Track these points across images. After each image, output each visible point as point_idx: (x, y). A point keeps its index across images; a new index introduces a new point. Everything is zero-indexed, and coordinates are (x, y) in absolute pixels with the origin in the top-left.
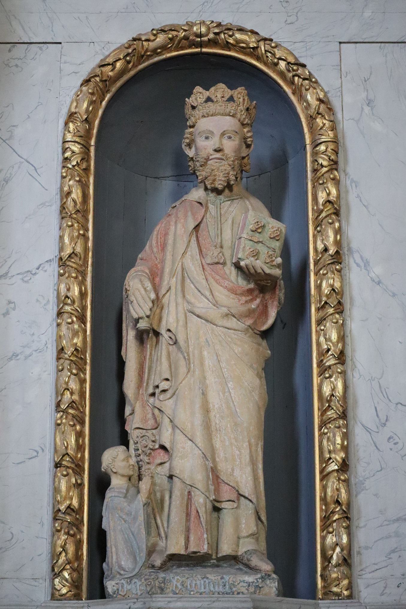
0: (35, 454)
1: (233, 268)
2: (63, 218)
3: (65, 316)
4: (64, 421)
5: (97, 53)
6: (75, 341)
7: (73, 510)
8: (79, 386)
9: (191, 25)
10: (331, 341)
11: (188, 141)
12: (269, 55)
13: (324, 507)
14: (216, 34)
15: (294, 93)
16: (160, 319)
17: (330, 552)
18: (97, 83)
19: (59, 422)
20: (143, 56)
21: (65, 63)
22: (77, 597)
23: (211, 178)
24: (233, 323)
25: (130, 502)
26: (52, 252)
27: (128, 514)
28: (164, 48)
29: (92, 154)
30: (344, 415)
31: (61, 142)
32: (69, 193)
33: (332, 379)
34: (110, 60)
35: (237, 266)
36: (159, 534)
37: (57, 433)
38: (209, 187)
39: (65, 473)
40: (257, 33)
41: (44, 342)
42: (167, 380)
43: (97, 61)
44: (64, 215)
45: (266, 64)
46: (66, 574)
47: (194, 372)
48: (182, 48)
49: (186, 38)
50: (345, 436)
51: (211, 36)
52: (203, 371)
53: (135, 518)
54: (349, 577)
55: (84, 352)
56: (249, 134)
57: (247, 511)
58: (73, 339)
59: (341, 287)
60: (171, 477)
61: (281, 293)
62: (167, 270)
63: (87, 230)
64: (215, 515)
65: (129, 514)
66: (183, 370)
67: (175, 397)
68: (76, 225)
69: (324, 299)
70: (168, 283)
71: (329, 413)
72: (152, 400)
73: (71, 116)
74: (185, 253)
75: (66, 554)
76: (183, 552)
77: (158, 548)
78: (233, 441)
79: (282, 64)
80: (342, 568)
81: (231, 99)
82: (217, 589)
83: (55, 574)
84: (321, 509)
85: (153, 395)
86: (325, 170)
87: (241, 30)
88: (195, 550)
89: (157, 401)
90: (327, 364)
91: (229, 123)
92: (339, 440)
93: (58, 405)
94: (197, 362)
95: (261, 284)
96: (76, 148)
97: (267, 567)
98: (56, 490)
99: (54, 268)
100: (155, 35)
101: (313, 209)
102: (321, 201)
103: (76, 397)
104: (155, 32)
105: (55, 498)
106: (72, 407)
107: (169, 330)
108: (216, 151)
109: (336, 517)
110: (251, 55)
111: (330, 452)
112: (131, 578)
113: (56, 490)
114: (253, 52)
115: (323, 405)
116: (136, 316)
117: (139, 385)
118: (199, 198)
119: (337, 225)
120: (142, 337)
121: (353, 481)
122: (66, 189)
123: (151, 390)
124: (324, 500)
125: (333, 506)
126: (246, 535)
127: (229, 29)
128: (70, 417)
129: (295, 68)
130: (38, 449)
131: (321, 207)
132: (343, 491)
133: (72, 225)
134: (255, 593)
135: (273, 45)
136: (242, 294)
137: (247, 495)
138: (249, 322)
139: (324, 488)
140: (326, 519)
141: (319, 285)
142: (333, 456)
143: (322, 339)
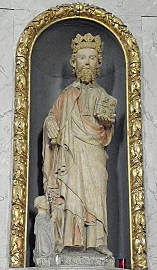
0: (3, 199)
1: (94, 118)
2: (16, 92)
3: (18, 136)
4: (17, 184)
5: (31, 16)
6: (23, 147)
7: (20, 225)
8: (23, 168)
9: (75, 5)
10: (137, 152)
11: (73, 59)
12: (110, 21)
13: (134, 227)
14: (86, 9)
15: (121, 40)
16: (61, 140)
17: (137, 247)
18: (31, 29)
19: (15, 184)
20: (52, 18)
21: (16, 19)
22: (22, 266)
23: (84, 77)
24: (94, 142)
25: (48, 221)
26: (11, 107)
27: (46, 227)
28: (62, 15)
29: (30, 63)
30: (142, 186)
31: (15, 57)
32: (20, 80)
33: (138, 169)
34: (38, 19)
35: (96, 117)
36: (60, 237)
37: (14, 189)
38: (83, 81)
39: (17, 208)
40: (105, 10)
41: (7, 148)
42: (64, 166)
43: (32, 18)
44: (17, 90)
45: (108, 25)
46: (17, 255)
47: (77, 163)
48: (71, 16)
49: (73, 11)
50: (143, 195)
51: (84, 10)
52: (81, 163)
53: (50, 229)
54: (146, 259)
55: (26, 153)
56: (101, 58)
57: (100, 227)
58: (22, 147)
59: (141, 128)
60: (65, 211)
61: (113, 129)
62: (64, 118)
63: (28, 98)
64: (85, 228)
65: (47, 227)
66: (72, 162)
67: (68, 174)
68: (23, 95)
69: (134, 133)
70: (65, 123)
71: (136, 184)
72: (56, 175)
73: (20, 45)
74: (72, 110)
75: (17, 245)
76: (71, 245)
77: (59, 243)
78: (94, 195)
79: (116, 26)
80: (143, 255)
81: (94, 41)
82: (87, 263)
83: (11, 254)
84: (133, 228)
85: (57, 173)
86: (135, 75)
87: (98, 8)
88: (77, 244)
89: (59, 176)
90: (135, 162)
91: (92, 52)
92: (141, 196)
93: (15, 176)
94: (78, 160)
95: (105, 125)
96: (23, 60)
97: (110, 253)
98: (13, 216)
99: (12, 115)
100: (58, 8)
101: (129, 93)
102: (133, 89)
103: (22, 173)
104: (58, 7)
105: (12, 219)
106: (21, 178)
107: (65, 144)
108: (86, 64)
109: (140, 231)
110: (102, 20)
111: (136, 201)
112: (48, 257)
113: (13, 216)
114: (103, 19)
115: (133, 181)
116: (50, 138)
117: (51, 169)
118: (78, 86)
119: (140, 100)
120: (52, 147)
121: (146, 215)
122: (18, 78)
123: (56, 171)
124: (134, 223)
125: (138, 226)
126: (99, 238)
127: (93, 8)
128: (20, 182)
129: (122, 27)
130: (4, 196)
131: (133, 92)
132: (143, 219)
133: (21, 95)
134: (104, 265)
135: (113, 16)
136: (97, 130)
137: (100, 220)
138: (101, 142)
139: (134, 218)
140: (134, 232)
141: (131, 127)
142: (138, 203)
143: (132, 151)
